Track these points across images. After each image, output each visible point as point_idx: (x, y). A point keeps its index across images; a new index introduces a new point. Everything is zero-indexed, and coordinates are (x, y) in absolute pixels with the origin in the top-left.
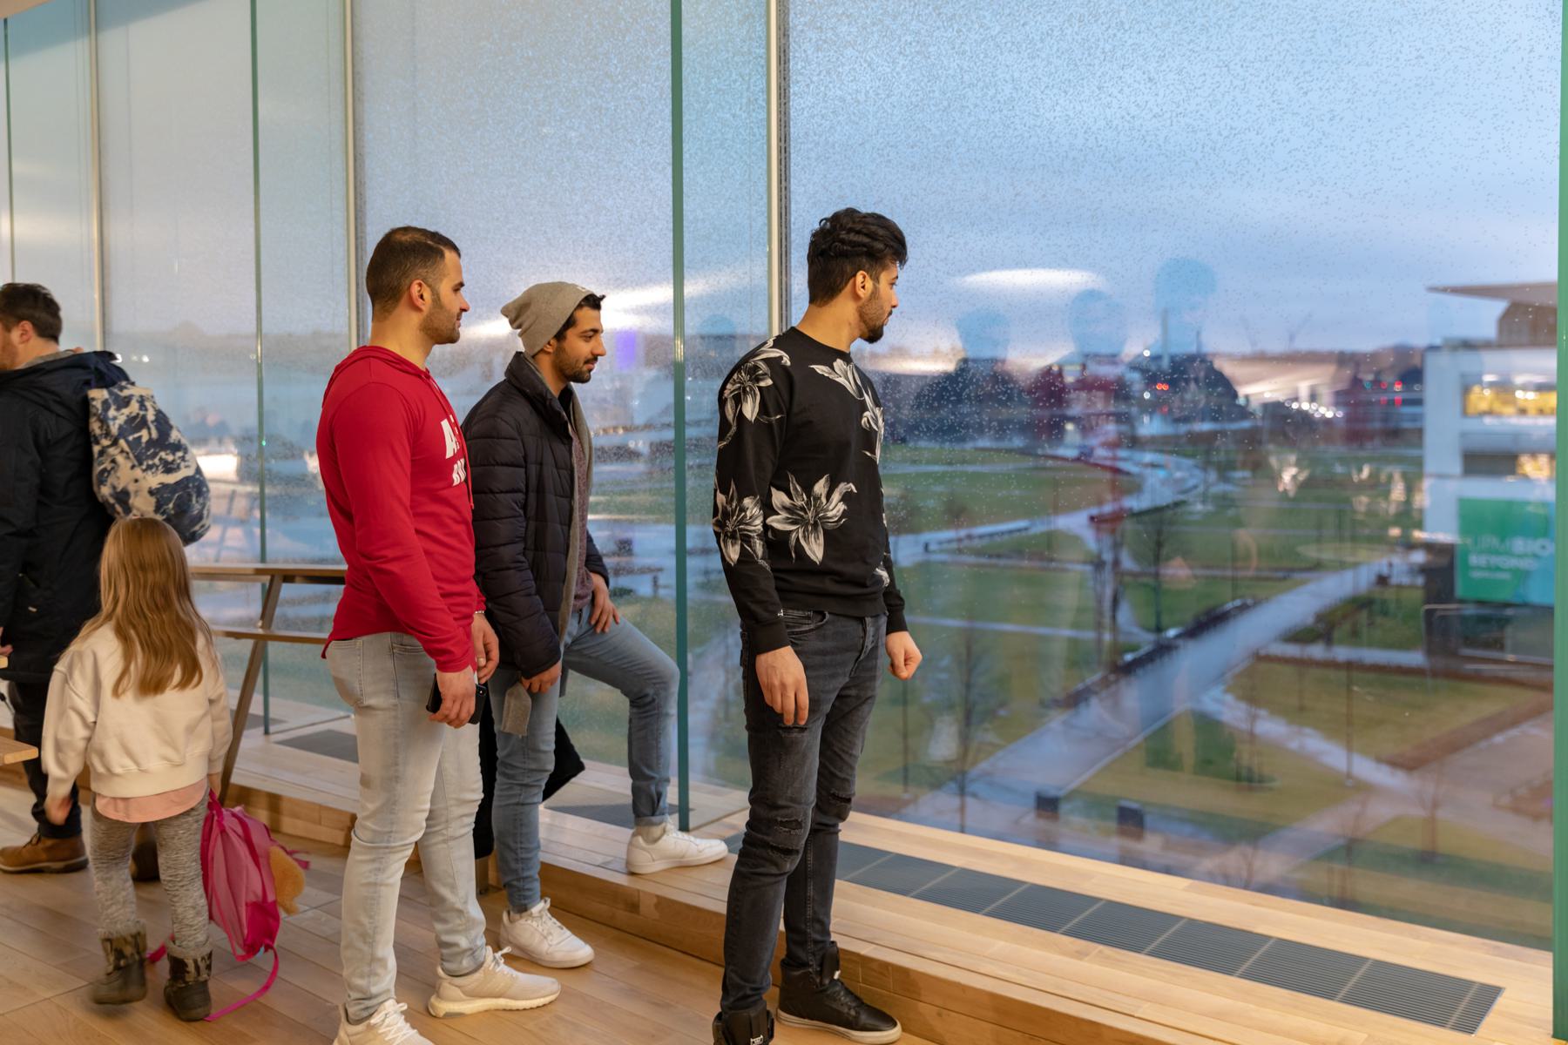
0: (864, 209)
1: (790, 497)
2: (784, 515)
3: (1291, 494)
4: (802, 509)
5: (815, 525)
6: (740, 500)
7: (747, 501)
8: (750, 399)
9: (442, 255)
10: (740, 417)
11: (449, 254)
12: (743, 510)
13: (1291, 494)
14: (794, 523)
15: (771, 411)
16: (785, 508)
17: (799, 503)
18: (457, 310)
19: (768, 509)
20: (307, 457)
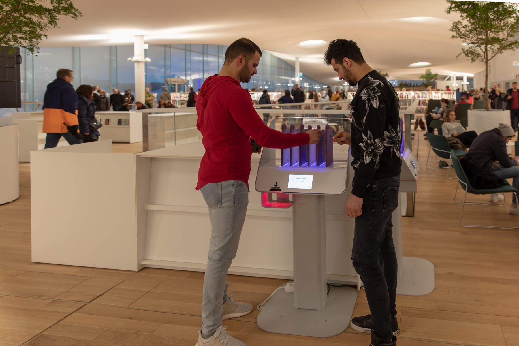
0: (348, 39)
1: (389, 132)
2: (388, 140)
3: (66, 77)
4: (394, 137)
5: (371, 152)
6: (374, 140)
7: (377, 140)
8: (375, 100)
9: (255, 52)
10: (371, 106)
11: (257, 53)
12: (375, 143)
13: (66, 77)
14: (391, 144)
15: (186, 90)
16: (388, 137)
17: (393, 135)
18: (252, 72)
19: (382, 141)
20: (336, 146)
